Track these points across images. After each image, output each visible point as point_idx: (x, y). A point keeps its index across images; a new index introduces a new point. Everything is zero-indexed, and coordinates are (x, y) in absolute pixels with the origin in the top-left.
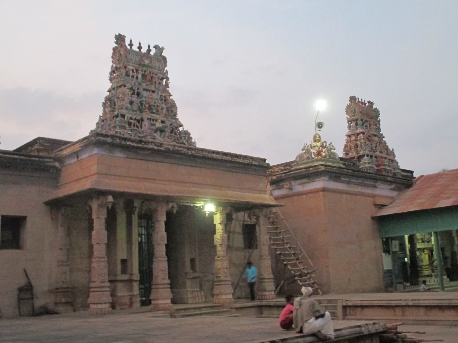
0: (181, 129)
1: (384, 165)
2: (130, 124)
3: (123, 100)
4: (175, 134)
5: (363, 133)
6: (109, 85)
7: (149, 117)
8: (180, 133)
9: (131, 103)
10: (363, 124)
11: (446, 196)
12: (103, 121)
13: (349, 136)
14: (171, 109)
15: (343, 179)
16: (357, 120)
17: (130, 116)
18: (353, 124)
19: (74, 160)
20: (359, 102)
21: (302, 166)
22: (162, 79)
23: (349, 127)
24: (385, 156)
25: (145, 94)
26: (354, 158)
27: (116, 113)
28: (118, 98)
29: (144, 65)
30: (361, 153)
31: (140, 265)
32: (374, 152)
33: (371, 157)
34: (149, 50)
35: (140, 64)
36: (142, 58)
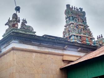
5: (73, 24)
10: (73, 19)
13: (66, 26)
15: (33, 42)
16: (70, 17)
26: (67, 38)
30: (71, 34)
32: (80, 34)
33: (77, 36)
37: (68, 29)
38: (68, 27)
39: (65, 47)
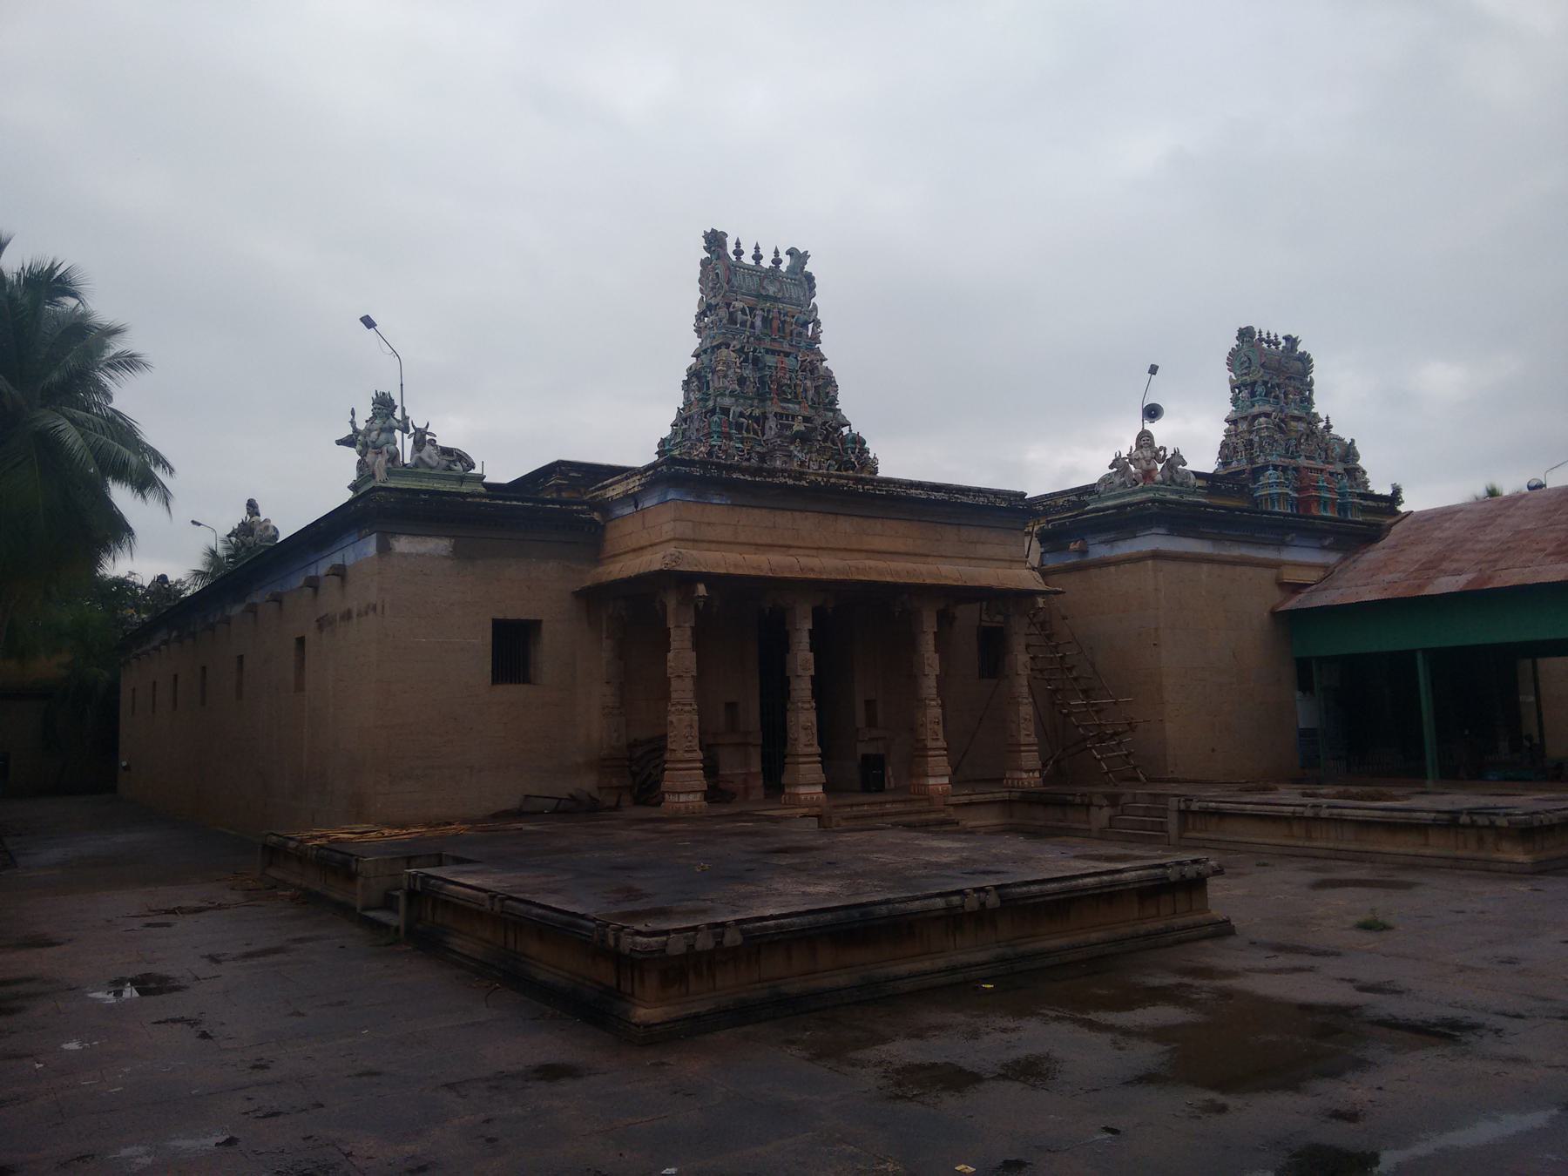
0: (845, 430)
1: (1317, 489)
2: (739, 427)
3: (725, 376)
4: (834, 443)
6: (694, 342)
7: (779, 410)
8: (844, 440)
9: (742, 381)
11: (1455, 565)
12: (685, 420)
14: (825, 389)
16: (1254, 383)
17: (739, 409)
18: (1245, 393)
19: (629, 510)
20: (1261, 340)
21: (1110, 503)
22: (805, 325)
23: (1235, 401)
24: (1320, 465)
25: (770, 360)
27: (711, 404)
28: (714, 372)
29: (767, 298)
30: (1261, 461)
31: (762, 714)
33: (1285, 469)
34: (777, 261)
35: (759, 296)
36: (761, 280)
37: (1247, 436)
38: (1243, 426)
39: (1288, 538)
